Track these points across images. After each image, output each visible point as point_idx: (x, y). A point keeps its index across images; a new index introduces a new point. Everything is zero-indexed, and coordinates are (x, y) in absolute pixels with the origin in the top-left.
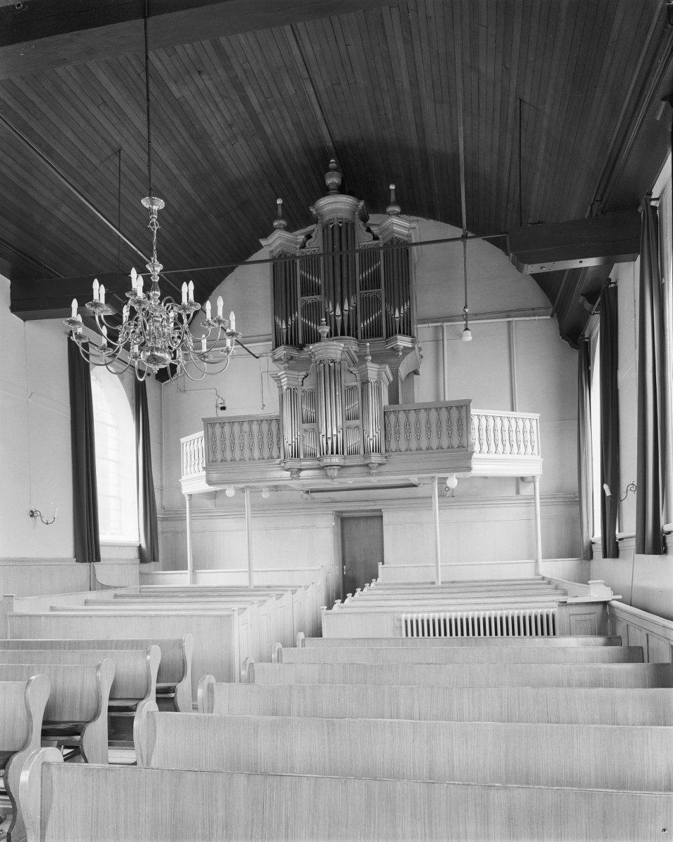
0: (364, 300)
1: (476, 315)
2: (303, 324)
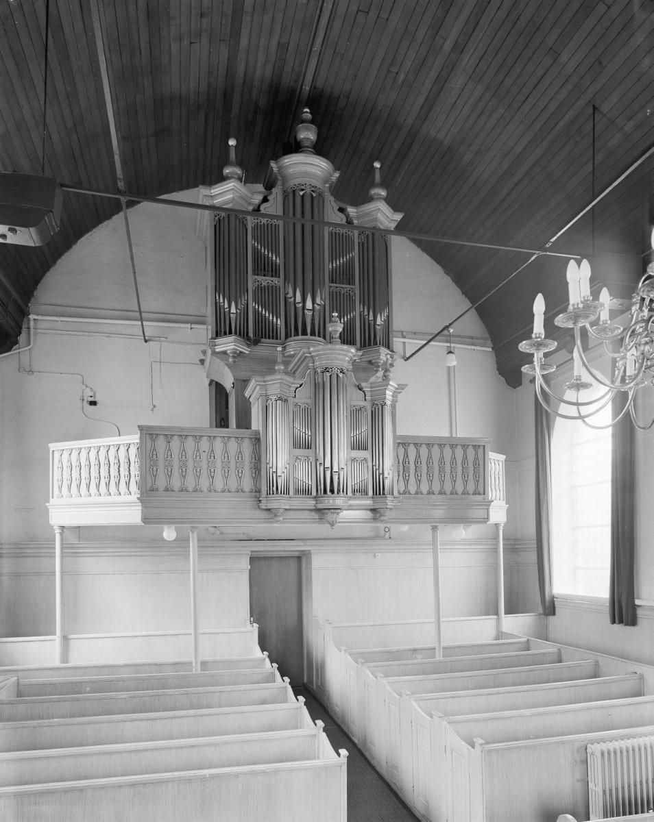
0: (332, 295)
1: (415, 333)
2: (255, 310)
